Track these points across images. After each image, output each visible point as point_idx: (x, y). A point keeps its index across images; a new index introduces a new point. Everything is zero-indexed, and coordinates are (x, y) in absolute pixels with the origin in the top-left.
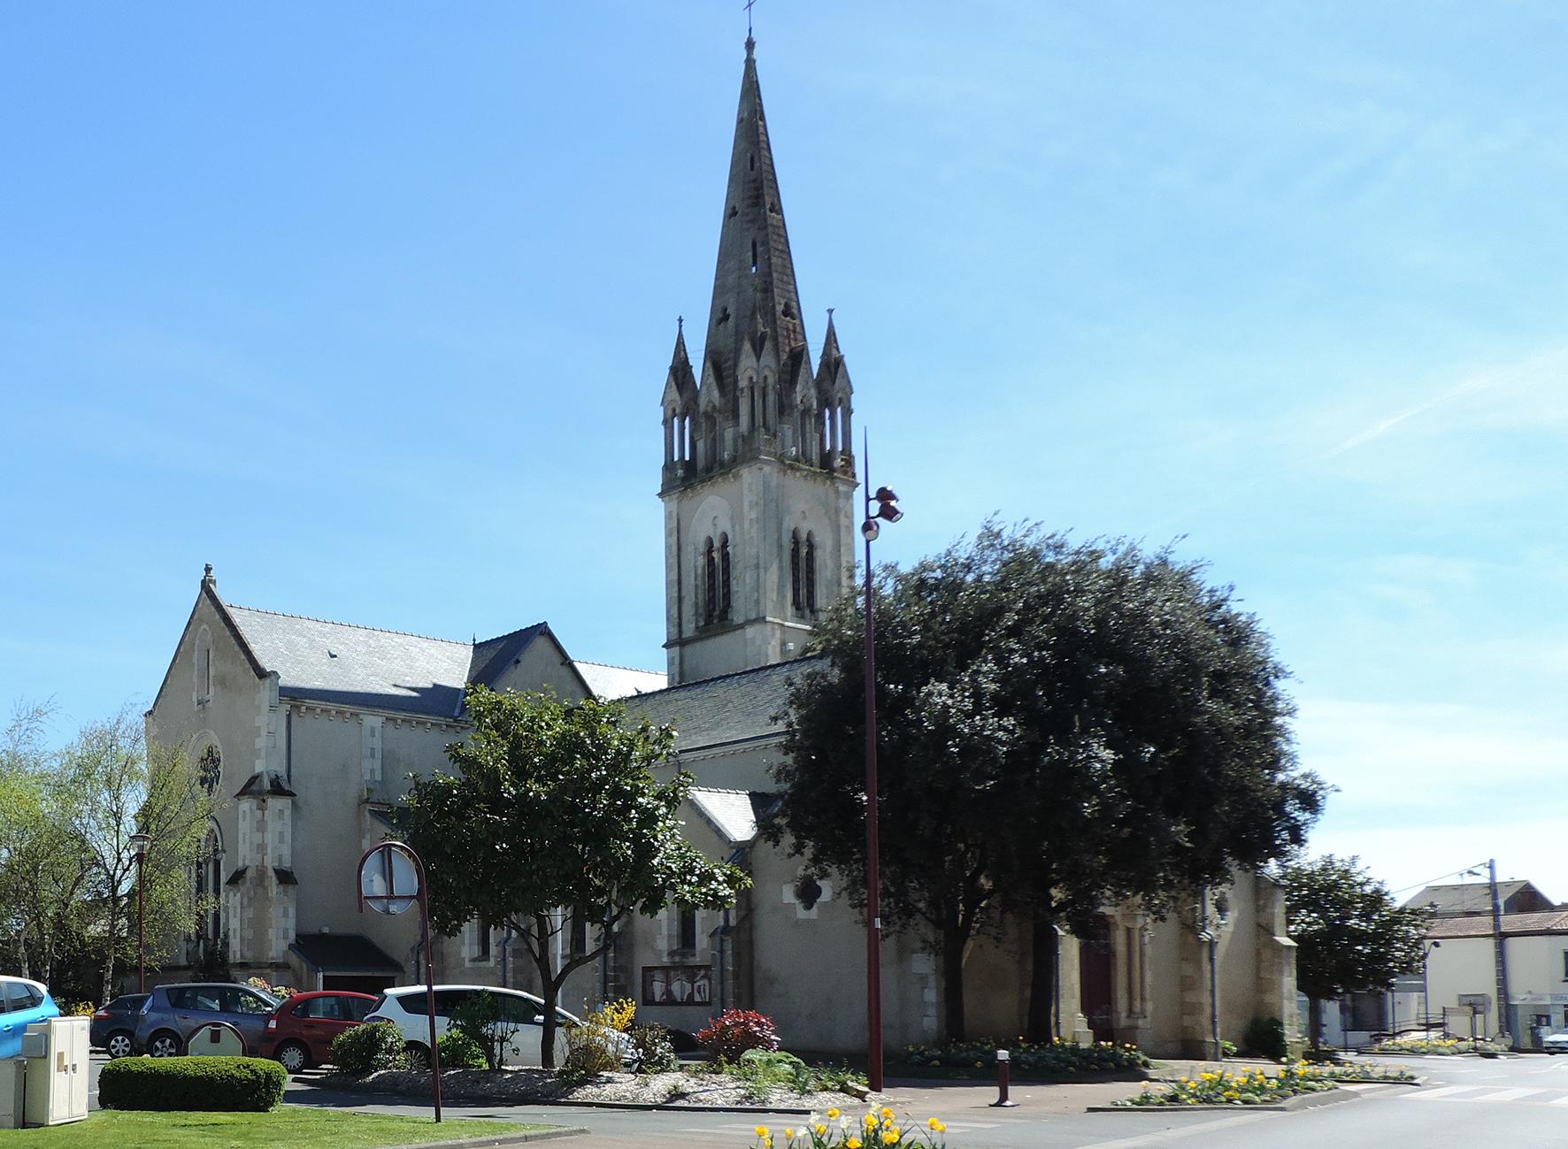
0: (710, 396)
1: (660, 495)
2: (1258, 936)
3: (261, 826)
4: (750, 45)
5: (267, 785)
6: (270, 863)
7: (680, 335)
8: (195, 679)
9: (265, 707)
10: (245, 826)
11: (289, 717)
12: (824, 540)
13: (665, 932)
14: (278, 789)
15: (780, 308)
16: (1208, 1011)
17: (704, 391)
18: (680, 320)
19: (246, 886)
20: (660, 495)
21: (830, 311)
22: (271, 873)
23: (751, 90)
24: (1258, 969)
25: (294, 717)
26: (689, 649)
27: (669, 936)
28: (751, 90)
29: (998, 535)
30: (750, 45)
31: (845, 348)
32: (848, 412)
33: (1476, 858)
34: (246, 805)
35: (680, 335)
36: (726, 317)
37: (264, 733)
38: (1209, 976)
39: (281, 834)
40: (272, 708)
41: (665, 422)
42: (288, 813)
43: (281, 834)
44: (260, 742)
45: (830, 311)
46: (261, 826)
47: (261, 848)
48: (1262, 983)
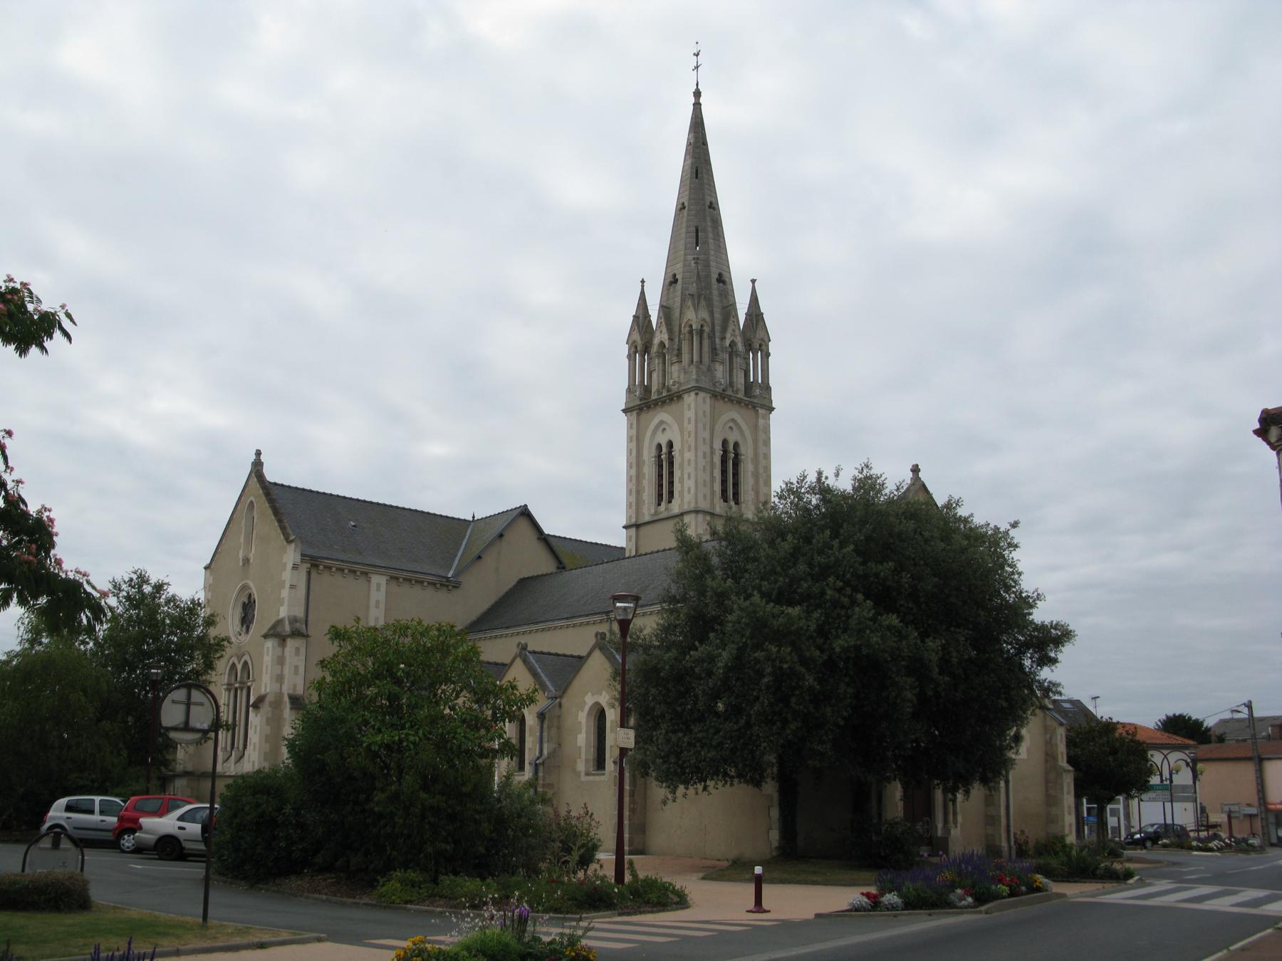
0: (661, 336)
1: (624, 411)
2: (1046, 761)
3: (281, 661)
4: (697, 94)
5: (288, 628)
6: (286, 689)
7: (643, 293)
8: (242, 540)
9: (290, 566)
10: (268, 659)
11: (309, 573)
12: (747, 451)
13: (583, 756)
14: (296, 634)
15: (715, 276)
16: (1003, 821)
17: (658, 333)
18: (643, 282)
19: (266, 708)
20: (624, 411)
21: (753, 281)
22: (286, 699)
23: (697, 125)
24: (1047, 787)
25: (314, 574)
26: (643, 530)
27: (587, 760)
28: (697, 125)
29: (131, 580)
30: (697, 94)
31: (764, 307)
32: (767, 355)
33: (1238, 699)
34: (270, 644)
35: (643, 293)
36: (675, 281)
37: (287, 585)
38: (99, 833)
39: (296, 668)
40: (295, 567)
41: (629, 357)
42: (303, 650)
43: (296, 668)
44: (285, 593)
45: (753, 281)
46: (281, 661)
47: (280, 678)
48: (1051, 800)
